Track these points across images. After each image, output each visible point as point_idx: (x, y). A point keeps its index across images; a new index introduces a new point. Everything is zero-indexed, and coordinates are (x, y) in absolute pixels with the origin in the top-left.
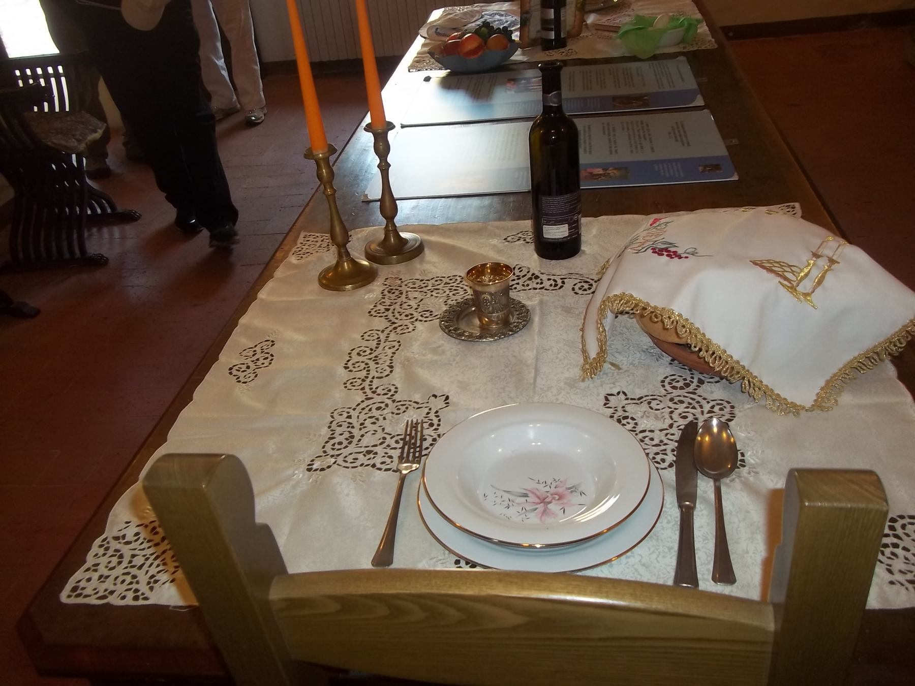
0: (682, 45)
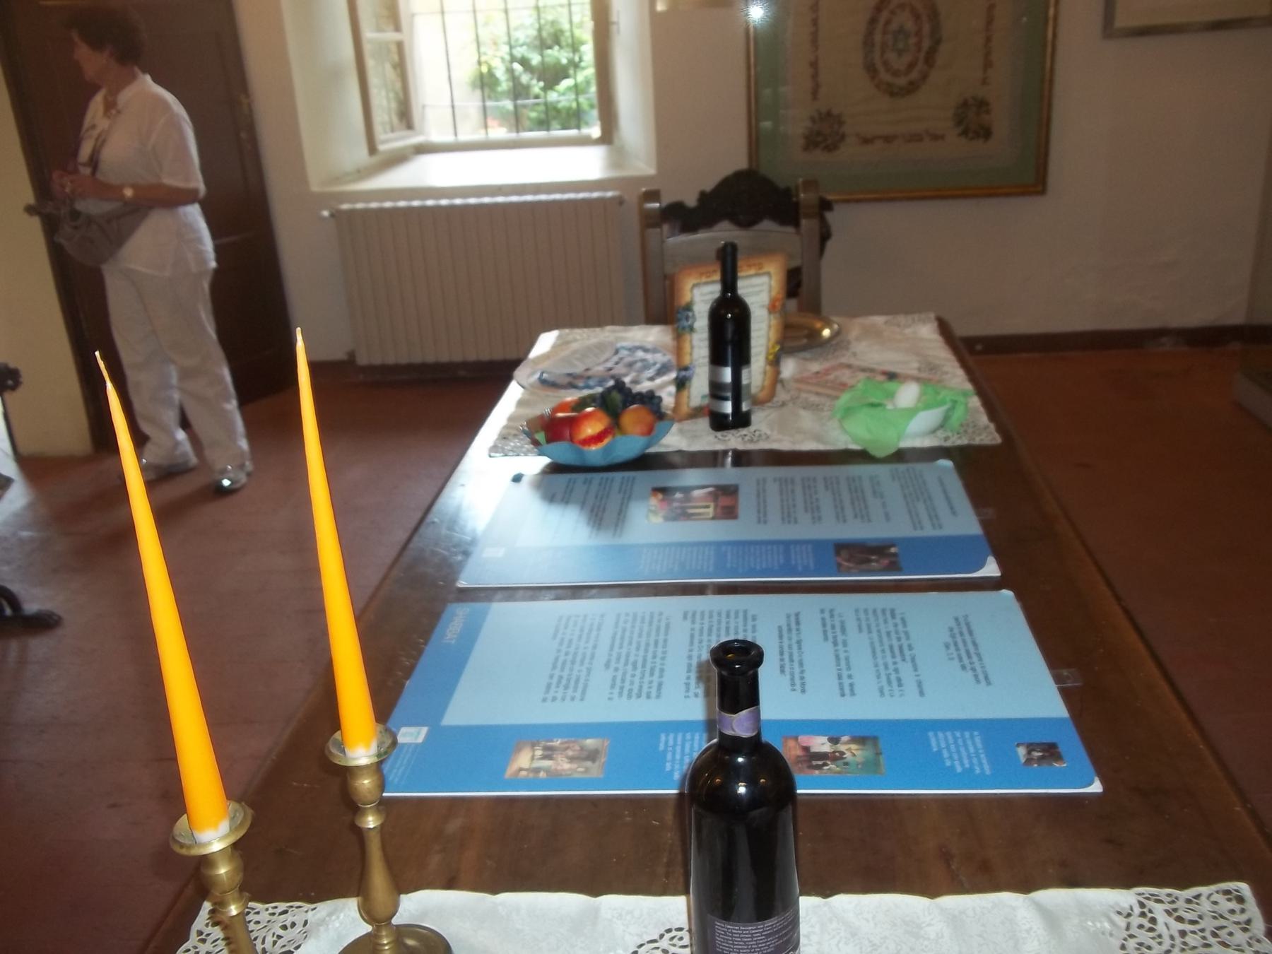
0: (941, 434)
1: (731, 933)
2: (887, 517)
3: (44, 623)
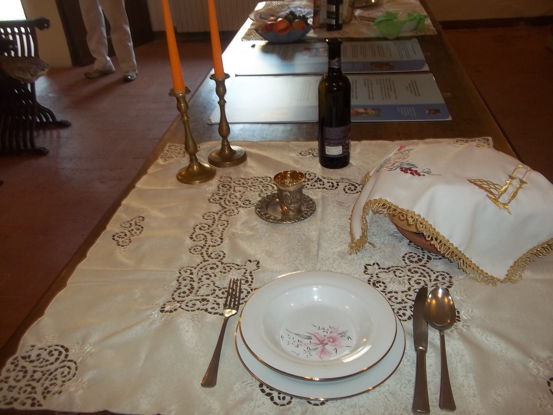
1: (331, 131)
2: (396, 98)
3: (64, 125)
